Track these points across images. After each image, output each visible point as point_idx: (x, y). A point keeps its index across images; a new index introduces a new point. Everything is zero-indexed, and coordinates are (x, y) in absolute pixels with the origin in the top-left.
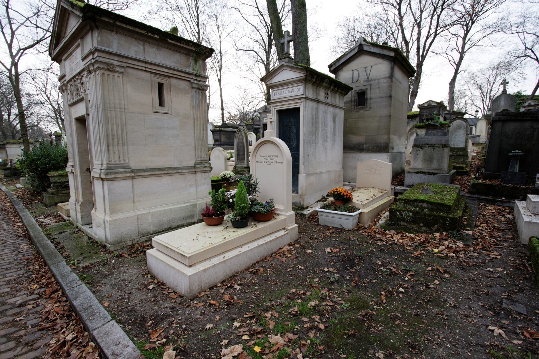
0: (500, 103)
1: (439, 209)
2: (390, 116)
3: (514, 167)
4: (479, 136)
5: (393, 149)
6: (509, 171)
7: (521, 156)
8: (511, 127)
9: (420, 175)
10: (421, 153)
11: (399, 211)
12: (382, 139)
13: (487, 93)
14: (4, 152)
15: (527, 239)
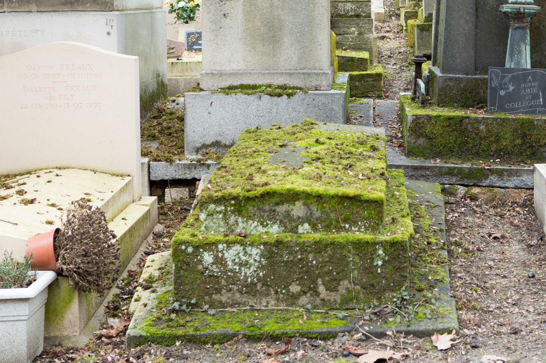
1: (346, 220)
3: (520, 52)
6: (507, 66)
9: (241, 97)
11: (210, 246)
14: (152, 179)
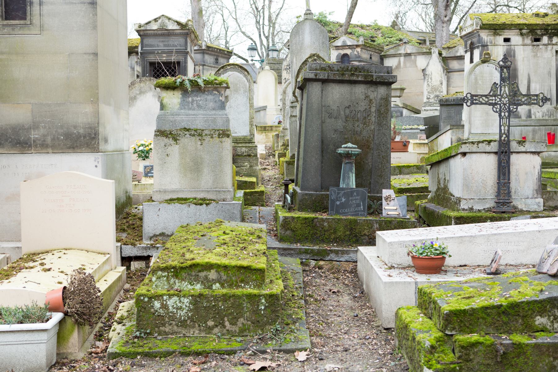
0: (303, 40)
1: (242, 281)
2: (96, 54)
3: (349, 178)
4: (264, 108)
5: (106, 141)
6: (341, 186)
7: (357, 155)
8: (337, 94)
9: (177, 205)
10: (175, 149)
11: (158, 297)
12: (79, 116)
13: (263, 8)
15: (392, 315)
